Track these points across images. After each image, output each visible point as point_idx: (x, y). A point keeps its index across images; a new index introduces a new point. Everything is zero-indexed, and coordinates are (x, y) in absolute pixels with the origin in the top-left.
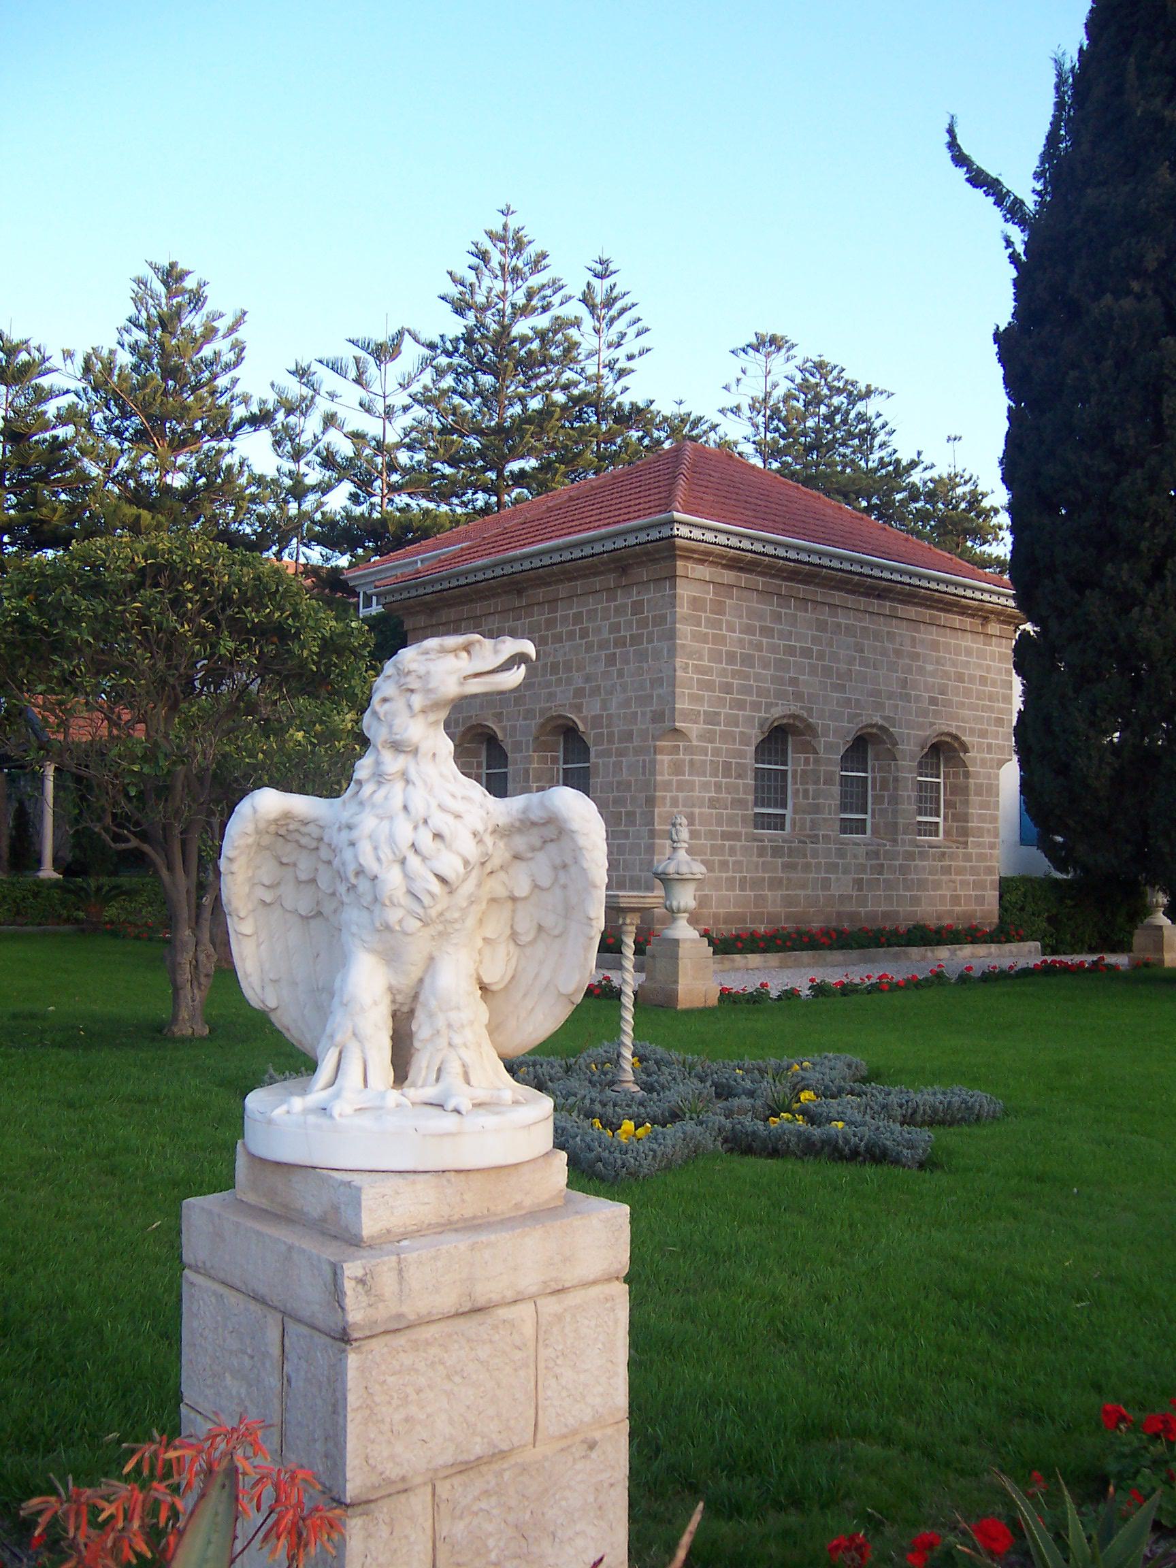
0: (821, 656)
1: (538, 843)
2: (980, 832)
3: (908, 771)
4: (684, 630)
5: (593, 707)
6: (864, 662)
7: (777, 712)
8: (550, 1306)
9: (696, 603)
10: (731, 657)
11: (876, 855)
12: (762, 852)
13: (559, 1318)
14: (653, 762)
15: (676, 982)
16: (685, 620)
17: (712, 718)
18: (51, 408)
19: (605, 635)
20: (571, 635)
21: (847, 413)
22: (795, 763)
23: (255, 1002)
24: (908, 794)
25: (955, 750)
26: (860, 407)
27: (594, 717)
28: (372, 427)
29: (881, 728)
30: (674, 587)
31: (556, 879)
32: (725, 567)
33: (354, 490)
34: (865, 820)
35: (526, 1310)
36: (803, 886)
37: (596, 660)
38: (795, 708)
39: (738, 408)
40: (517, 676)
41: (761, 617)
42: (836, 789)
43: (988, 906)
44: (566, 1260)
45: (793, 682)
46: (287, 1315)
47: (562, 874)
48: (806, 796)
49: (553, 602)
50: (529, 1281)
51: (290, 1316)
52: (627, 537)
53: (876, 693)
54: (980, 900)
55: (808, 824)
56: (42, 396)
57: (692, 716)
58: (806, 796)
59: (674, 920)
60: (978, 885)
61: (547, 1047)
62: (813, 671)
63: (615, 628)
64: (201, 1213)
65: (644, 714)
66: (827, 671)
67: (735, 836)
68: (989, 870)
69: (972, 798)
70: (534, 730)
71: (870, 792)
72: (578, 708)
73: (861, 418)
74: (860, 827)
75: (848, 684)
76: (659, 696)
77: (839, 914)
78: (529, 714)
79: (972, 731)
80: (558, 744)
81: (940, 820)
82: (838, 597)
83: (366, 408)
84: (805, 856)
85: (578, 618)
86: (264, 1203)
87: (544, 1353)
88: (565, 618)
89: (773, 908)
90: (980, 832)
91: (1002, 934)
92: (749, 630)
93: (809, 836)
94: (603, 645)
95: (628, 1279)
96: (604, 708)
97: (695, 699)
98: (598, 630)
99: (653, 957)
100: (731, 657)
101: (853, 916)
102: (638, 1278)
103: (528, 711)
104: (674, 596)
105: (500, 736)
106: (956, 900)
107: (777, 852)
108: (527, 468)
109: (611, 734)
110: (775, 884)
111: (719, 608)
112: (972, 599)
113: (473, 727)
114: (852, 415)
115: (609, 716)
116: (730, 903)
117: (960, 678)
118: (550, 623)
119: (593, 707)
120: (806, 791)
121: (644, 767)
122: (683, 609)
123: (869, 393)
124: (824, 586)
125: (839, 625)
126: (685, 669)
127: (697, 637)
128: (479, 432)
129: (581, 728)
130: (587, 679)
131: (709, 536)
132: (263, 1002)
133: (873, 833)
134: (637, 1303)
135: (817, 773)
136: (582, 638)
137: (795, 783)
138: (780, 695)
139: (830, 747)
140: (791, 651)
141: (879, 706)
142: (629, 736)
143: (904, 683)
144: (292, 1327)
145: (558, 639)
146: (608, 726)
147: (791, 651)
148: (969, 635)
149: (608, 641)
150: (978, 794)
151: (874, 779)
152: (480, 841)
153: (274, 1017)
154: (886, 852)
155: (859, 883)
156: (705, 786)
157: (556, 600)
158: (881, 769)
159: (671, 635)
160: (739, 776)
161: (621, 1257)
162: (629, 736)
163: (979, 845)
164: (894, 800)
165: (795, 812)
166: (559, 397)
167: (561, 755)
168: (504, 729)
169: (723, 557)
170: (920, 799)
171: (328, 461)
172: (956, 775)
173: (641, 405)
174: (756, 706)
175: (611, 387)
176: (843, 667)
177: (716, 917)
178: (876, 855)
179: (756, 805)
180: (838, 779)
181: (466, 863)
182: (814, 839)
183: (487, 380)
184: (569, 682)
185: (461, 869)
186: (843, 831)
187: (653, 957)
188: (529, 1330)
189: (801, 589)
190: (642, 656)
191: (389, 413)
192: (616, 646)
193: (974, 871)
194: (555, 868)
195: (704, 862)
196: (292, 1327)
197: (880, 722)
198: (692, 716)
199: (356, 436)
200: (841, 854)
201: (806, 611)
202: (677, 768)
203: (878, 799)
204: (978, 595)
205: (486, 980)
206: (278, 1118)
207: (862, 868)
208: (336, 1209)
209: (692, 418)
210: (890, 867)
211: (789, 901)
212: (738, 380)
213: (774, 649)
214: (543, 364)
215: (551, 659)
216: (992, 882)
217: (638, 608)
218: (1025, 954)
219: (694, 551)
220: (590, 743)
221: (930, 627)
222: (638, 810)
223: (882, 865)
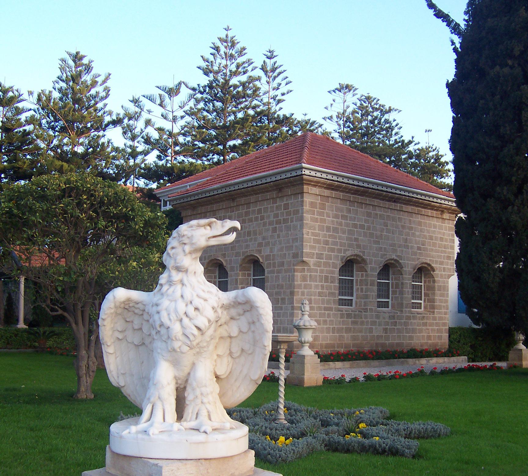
0: (369, 228)
1: (242, 312)
2: (440, 307)
4: (307, 217)
5: (266, 251)
6: (388, 231)
7: (349, 253)
9: (312, 204)
10: (328, 229)
11: (393, 317)
12: (342, 316)
14: (293, 276)
15: (304, 374)
16: (308, 212)
17: (319, 256)
18: (23, 117)
19: (272, 219)
20: (256, 219)
21: (380, 119)
22: (357, 276)
23: (114, 383)
24: (408, 290)
25: (429, 270)
26: (386, 116)
27: (267, 256)
28: (167, 125)
29: (396, 260)
30: (302, 197)
31: (250, 329)
32: (326, 188)
33: (159, 154)
36: (361, 331)
37: (268, 230)
38: (357, 252)
39: (331, 117)
40: (232, 237)
41: (342, 211)
42: (375, 288)
43: (443, 340)
45: (356, 240)
47: (252, 326)
48: (362, 291)
54: (440, 337)
55: (363, 303)
56: (19, 111)
57: (311, 255)
58: (362, 291)
59: (303, 346)
60: (439, 331)
61: (246, 404)
62: (365, 235)
63: (276, 216)
66: (371, 235)
68: (444, 324)
69: (437, 292)
71: (391, 289)
72: (260, 252)
73: (387, 121)
74: (386, 305)
76: (296, 246)
77: (377, 344)
78: (237, 254)
81: (422, 302)
82: (376, 202)
83: (164, 117)
85: (259, 211)
89: (347, 341)
90: (440, 307)
91: (450, 353)
92: (336, 216)
93: (363, 309)
96: (271, 252)
97: (312, 247)
99: (293, 363)
101: (383, 345)
103: (237, 253)
104: (303, 201)
105: (225, 264)
106: (429, 337)
107: (349, 316)
109: (274, 263)
110: (348, 330)
111: (323, 207)
112: (436, 203)
114: (383, 120)
115: (274, 255)
116: (328, 339)
117: (431, 238)
118: (247, 214)
119: (266, 251)
120: (362, 289)
121: (289, 278)
122: (307, 207)
123: (390, 110)
124: (370, 197)
125: (376, 214)
126: (308, 234)
127: (313, 220)
129: (261, 260)
131: (319, 175)
135: (367, 281)
136: (261, 220)
138: (350, 246)
139: (372, 269)
140: (355, 226)
141: (395, 251)
142: (282, 264)
145: (251, 220)
146: (273, 260)
147: (355, 226)
148: (435, 219)
149: (273, 221)
150: (439, 290)
152: (216, 311)
153: (123, 390)
154: (398, 316)
155: (385, 330)
156: (316, 287)
157: (250, 203)
158: (396, 279)
159: (301, 219)
160: (332, 282)
162: (282, 264)
163: (439, 313)
164: (402, 293)
165: (357, 298)
166: (251, 112)
168: (226, 261)
169: (325, 184)
170: (413, 292)
171: (147, 141)
172: (429, 281)
174: (339, 251)
175: (274, 107)
176: (379, 233)
177: (321, 345)
178: (393, 317)
179: (339, 295)
180: (376, 283)
181: (209, 321)
182: (366, 310)
183: (219, 104)
184: (255, 240)
185: (207, 324)
187: (293, 363)
190: (288, 228)
191: (174, 119)
194: (249, 323)
195: (316, 321)
197: (395, 258)
198: (311, 255)
199: (160, 130)
200: (378, 317)
201: (362, 208)
202: (304, 279)
203: (394, 292)
204: (439, 201)
205: (218, 374)
207: (387, 323)
209: (311, 122)
210: (399, 323)
211: (354, 338)
212: (332, 105)
213: (347, 225)
214: (244, 97)
216: (445, 329)
217: (286, 207)
218: (460, 362)
219: (312, 181)
220: (265, 267)
221: (417, 215)
222: (287, 297)
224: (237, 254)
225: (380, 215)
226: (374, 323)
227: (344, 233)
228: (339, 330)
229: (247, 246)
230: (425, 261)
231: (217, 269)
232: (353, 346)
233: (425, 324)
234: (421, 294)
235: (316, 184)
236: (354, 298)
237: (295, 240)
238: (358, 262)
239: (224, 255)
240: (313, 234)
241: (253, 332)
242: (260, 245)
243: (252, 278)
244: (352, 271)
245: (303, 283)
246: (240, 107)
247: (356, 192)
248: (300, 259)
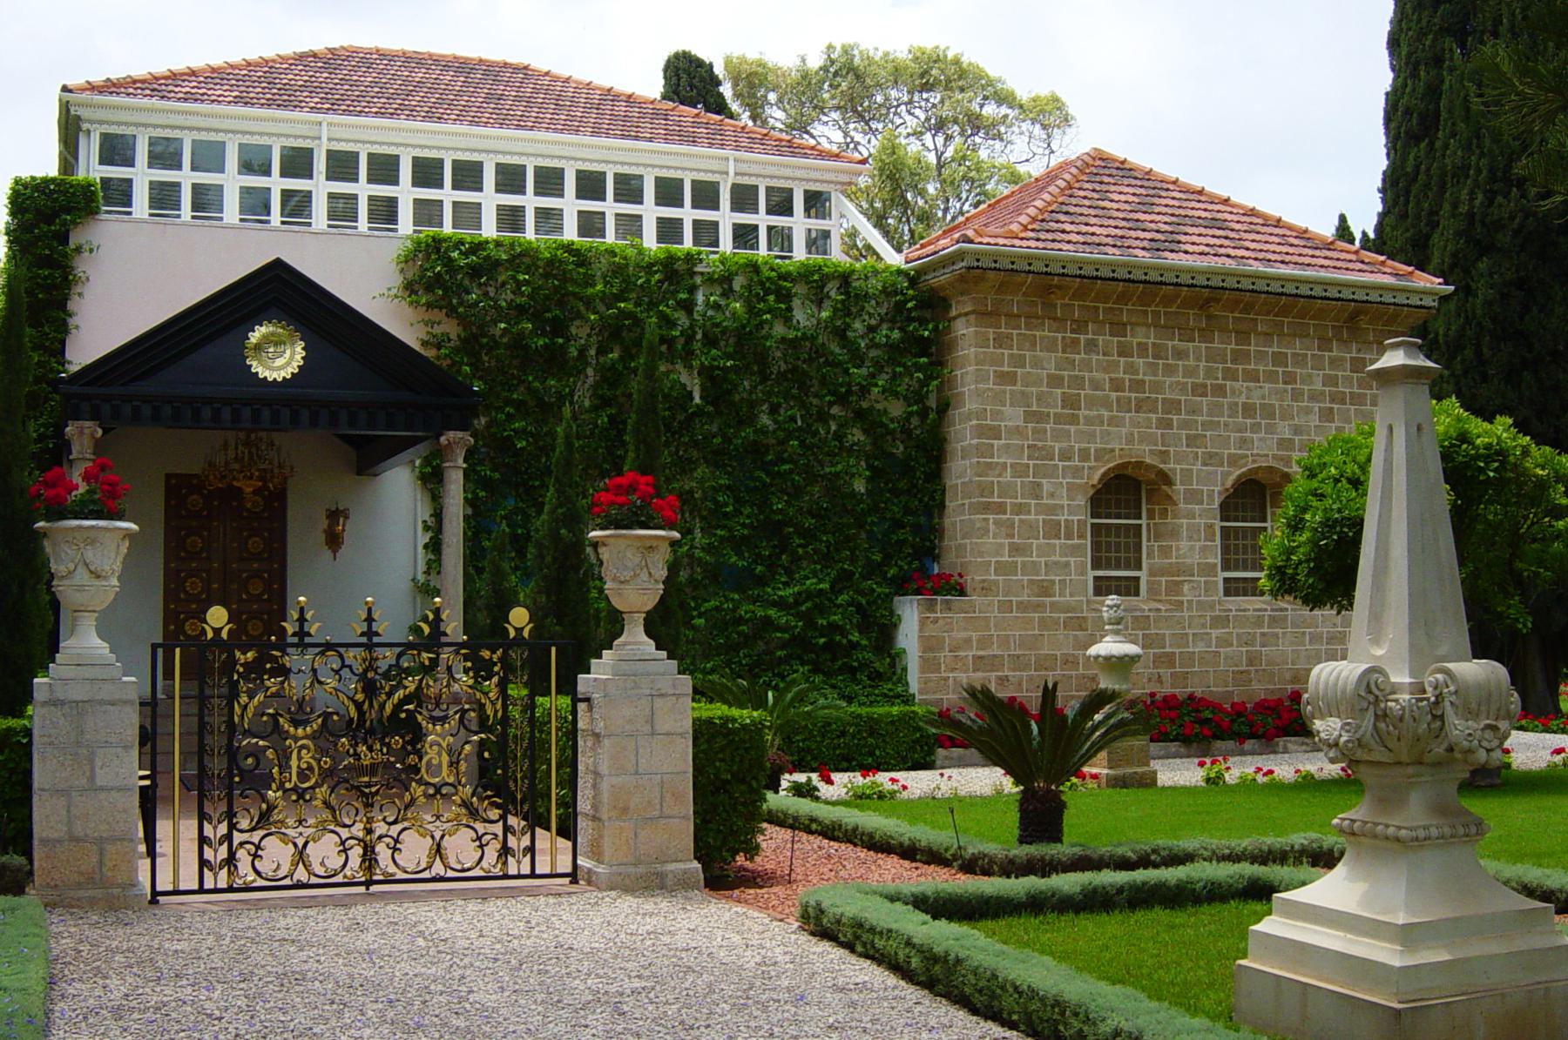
19: (1318, 386)
34: (1137, 579)
37: (1308, 411)
63: (1330, 381)
75: (1073, 428)
88: (1261, 356)
94: (1314, 397)
98: (1308, 379)
108: (721, 89)
130: (1297, 430)
137: (1149, 540)
165: (1152, 573)
184: (1270, 429)
186: (1227, 593)
192: (1333, 401)
215: (1243, 399)
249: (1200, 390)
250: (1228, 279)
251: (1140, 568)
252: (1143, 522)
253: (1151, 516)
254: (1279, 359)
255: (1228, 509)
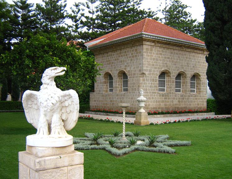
0: (171, 59)
1: (69, 98)
2: (203, 92)
3: (188, 80)
4: (145, 54)
5: (128, 69)
6: (180, 60)
7: (163, 69)
8: (70, 168)
9: (147, 49)
10: (154, 59)
11: (182, 96)
12: (160, 96)
13: (71, 170)
14: (139, 79)
15: (141, 120)
16: (145, 52)
17: (150, 71)
18: (31, 14)
19: (130, 55)
20: (124, 55)
21: (182, 11)
22: (166, 79)
23: (29, 122)
24: (189, 84)
25: (198, 76)
26: (185, 10)
27: (128, 71)
28: (90, 16)
29: (183, 72)
30: (143, 46)
31: (72, 103)
32: (152, 42)
33: (87, 28)
34: (180, 89)
35: (66, 168)
36: (168, 102)
37: (129, 60)
38: (166, 69)
39: (160, 10)
40: (64, 73)
41: (160, 52)
42: (174, 84)
43: (204, 105)
44: (72, 161)
45: (166, 63)
46: (30, 168)
47: (73, 103)
48: (169, 85)
49: (121, 49)
50: (66, 164)
51: (31, 169)
52: (140, 35)
53: (182, 65)
54: (203, 104)
55: (169, 90)
56: (29, 11)
57: (147, 70)
58: (169, 85)
59: (141, 108)
60: (203, 102)
61: (73, 129)
62: (170, 61)
63: (132, 54)
64: (21, 154)
65: (137, 70)
66: (173, 61)
67: (155, 93)
68: (205, 99)
69: (201, 85)
70: (118, 73)
71: (181, 84)
72: (126, 69)
73: (185, 12)
74: (179, 91)
76: (140, 67)
77: (175, 107)
78: (117, 70)
79: (201, 72)
80: (122, 75)
81: (195, 89)
82: (175, 48)
83: (90, 12)
84: (168, 96)
85: (125, 52)
86: (29, 152)
87: (69, 175)
89: (163, 106)
90: (203, 92)
91: (208, 110)
92: (157, 54)
93: (169, 93)
95: (83, 164)
96: (130, 69)
97: (147, 67)
99: (137, 115)
100: (154, 59)
101: (178, 108)
102: (85, 164)
103: (116, 70)
104: (143, 48)
105: (112, 74)
106: (198, 104)
107: (163, 95)
109: (131, 74)
110: (163, 102)
111: (151, 50)
112: (201, 47)
113: (106, 73)
114: (183, 11)
115: (131, 71)
116: (153, 105)
117: (199, 62)
118: (120, 53)
119: (128, 69)
120: (169, 84)
121: (138, 80)
122: (145, 50)
123: (186, 7)
124: (172, 46)
125: (175, 53)
126: (145, 61)
127: (147, 55)
128: (110, 16)
129: (126, 73)
131: (149, 37)
132: (45, 122)
133: (182, 92)
134: (84, 167)
135: (170, 81)
136: (126, 56)
137: (167, 83)
138: (163, 66)
139: (173, 76)
140: (165, 58)
141: (183, 68)
142: (135, 74)
143: (188, 64)
144: (31, 170)
145: (122, 56)
146: (131, 72)
147: (165, 58)
148: (201, 54)
149: (131, 56)
150: (202, 84)
151: (182, 82)
152: (59, 98)
153: (32, 124)
154: (184, 95)
155: (179, 101)
156: (149, 83)
157: (121, 49)
158: (183, 80)
159: (142, 55)
160: (156, 81)
161: (82, 161)
162: (135, 74)
163: (203, 94)
164: (186, 86)
165: (167, 88)
166: (126, 9)
167: (123, 78)
168: (112, 73)
169: (152, 40)
170: (191, 85)
171: (82, 22)
172: (198, 81)
173: (142, 10)
174: (159, 68)
175: (136, 7)
176: (176, 61)
177: (151, 108)
178: (182, 96)
179: (159, 87)
180: (175, 82)
181: (56, 101)
182: (170, 93)
183: (112, 6)
184: (124, 64)
185: (56, 102)
187: (137, 115)
188: (66, 171)
189: (167, 46)
190: (137, 59)
191: (93, 13)
193: (202, 99)
194: (72, 102)
195: (146, 98)
196: (31, 170)
197: (183, 71)
198: (147, 70)
199: (87, 17)
200: (176, 96)
201: (168, 50)
202: (144, 80)
203: (183, 86)
204: (202, 47)
205: (63, 119)
206: (30, 140)
207: (180, 99)
208: (37, 153)
209: (152, 12)
210: (185, 98)
211: (165, 105)
212: (160, 5)
213: (162, 57)
214: (123, 3)
216: (205, 101)
217: (136, 50)
218: (212, 115)
219: (146, 39)
220: (128, 76)
221: (193, 53)
222: (137, 88)
223: (184, 98)
224: (117, 70)
225: (176, 53)
226: (174, 98)
227: (161, 61)
228: (159, 102)
229: (121, 67)
230: (196, 72)
231: (109, 77)
232: (165, 108)
233: (196, 99)
234: (195, 86)
235: (148, 41)
236: (165, 88)
237: (140, 64)
238: (167, 73)
239: (111, 71)
240: (147, 61)
241: (73, 104)
242: (126, 66)
243: (123, 80)
244: (165, 77)
245: (143, 82)
246: (121, 7)
247: (165, 44)
248: (142, 72)
249: (116, 60)
250: (112, 43)
251: (195, 88)
252: (181, 81)
253: (196, 81)
254: (125, 52)
255: (177, 78)
